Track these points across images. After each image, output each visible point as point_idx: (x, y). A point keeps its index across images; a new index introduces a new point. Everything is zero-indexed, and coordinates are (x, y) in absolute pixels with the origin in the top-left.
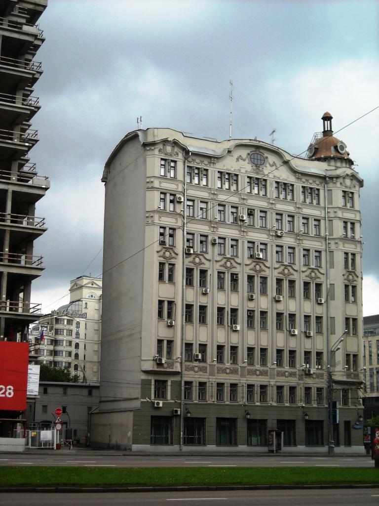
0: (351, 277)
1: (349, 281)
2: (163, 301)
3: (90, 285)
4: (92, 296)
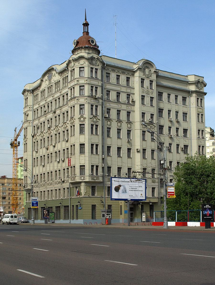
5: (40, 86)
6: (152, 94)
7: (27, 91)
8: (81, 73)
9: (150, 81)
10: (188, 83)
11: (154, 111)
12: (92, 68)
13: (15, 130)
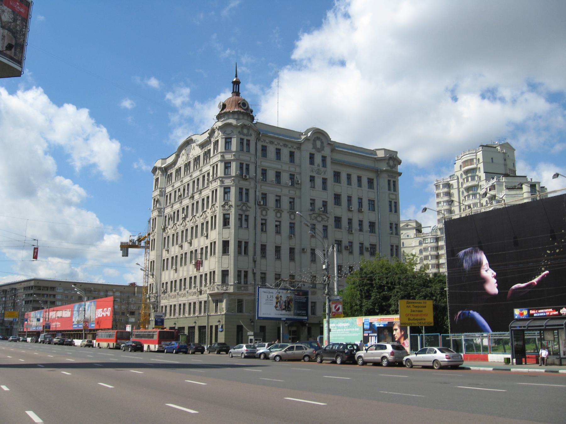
0: (244, 208)
8: (227, 145)
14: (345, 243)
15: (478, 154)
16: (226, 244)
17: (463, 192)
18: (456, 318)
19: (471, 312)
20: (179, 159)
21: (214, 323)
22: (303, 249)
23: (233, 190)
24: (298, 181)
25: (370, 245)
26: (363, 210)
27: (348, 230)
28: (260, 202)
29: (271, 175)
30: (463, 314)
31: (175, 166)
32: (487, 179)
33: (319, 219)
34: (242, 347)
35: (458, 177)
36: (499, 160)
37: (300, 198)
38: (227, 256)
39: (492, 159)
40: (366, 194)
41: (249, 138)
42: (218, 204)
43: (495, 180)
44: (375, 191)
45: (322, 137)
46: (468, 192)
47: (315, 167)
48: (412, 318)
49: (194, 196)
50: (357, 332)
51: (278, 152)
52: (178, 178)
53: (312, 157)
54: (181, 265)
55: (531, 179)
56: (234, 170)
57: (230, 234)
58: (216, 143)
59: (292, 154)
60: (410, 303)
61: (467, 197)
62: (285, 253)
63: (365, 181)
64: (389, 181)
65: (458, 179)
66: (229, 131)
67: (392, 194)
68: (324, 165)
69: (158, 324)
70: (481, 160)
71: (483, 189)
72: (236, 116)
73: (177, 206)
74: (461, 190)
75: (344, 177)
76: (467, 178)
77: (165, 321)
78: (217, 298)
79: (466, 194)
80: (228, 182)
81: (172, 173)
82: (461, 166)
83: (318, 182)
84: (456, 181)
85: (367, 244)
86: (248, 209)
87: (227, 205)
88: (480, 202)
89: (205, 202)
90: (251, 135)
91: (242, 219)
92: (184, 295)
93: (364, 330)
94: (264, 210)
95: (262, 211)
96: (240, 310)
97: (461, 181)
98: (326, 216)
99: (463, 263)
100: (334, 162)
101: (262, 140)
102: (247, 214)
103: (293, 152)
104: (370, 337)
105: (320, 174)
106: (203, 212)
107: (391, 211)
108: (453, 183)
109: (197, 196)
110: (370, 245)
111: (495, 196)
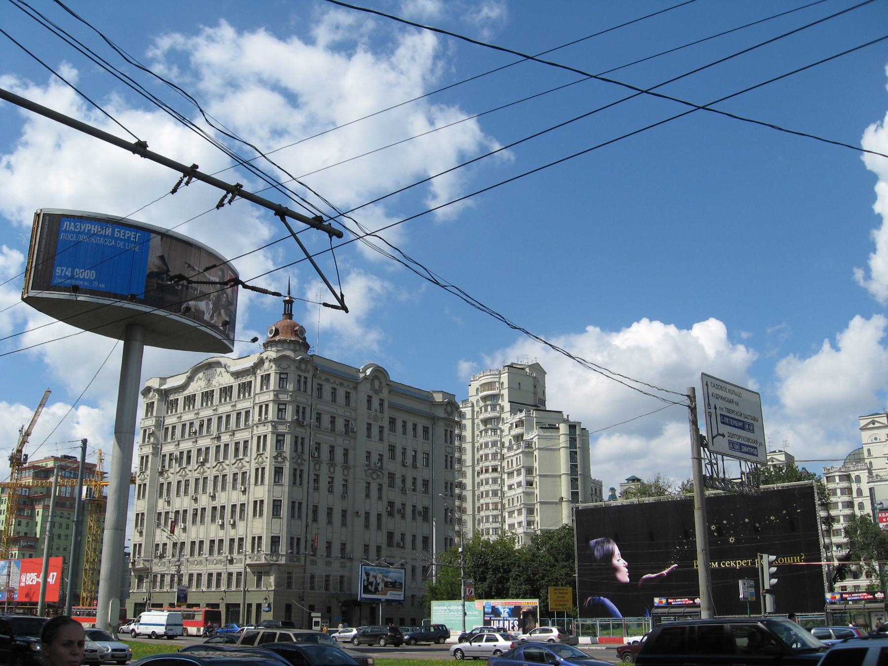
0: (299, 461)
1: (298, 464)
2: (489, 503)
3: (871, 426)
4: (876, 439)
5: (184, 387)
6: (382, 421)
7: (154, 390)
8: (281, 382)
9: (380, 399)
10: (434, 404)
11: (384, 449)
12: (300, 376)
13: (20, 431)
14: (398, 505)
15: (502, 376)
16: (276, 505)
17: (478, 425)
18: (586, 603)
19: (602, 598)
20: (192, 383)
21: (254, 600)
22: (357, 513)
23: (288, 439)
24: (353, 429)
25: (423, 507)
26: (418, 466)
27: (402, 490)
28: (314, 454)
29: (326, 421)
30: (593, 600)
31: (183, 391)
32: (513, 411)
33: (375, 476)
34: (351, 631)
35: (473, 404)
36: (528, 385)
37: (354, 449)
38: (278, 519)
39: (519, 384)
40: (422, 446)
41: (306, 375)
42: (268, 453)
43: (523, 414)
44: (430, 442)
45: (380, 376)
46: (486, 425)
47: (373, 413)
48: (558, 603)
49: (220, 436)
50: (476, 616)
51: (334, 392)
52: (189, 408)
53: (369, 400)
54: (194, 522)
55: (568, 416)
56: (289, 415)
57: (283, 492)
58: (266, 378)
59: (348, 396)
60: (557, 589)
61: (483, 432)
62: (337, 516)
63: (420, 430)
64: (446, 430)
65: (473, 406)
66: (285, 364)
67: (449, 447)
68: (382, 411)
69: (181, 600)
70: (506, 385)
71: (507, 423)
72: (292, 346)
73: (186, 446)
74: (476, 421)
75: (399, 424)
76: (486, 406)
77: (189, 594)
78: (260, 571)
79: (482, 427)
80: (282, 429)
81: (178, 399)
82: (477, 389)
83: (375, 431)
84: (470, 408)
85: (420, 508)
86: (303, 462)
87: (281, 456)
88: (501, 441)
89: (241, 448)
90: (309, 371)
91: (297, 476)
92: (200, 563)
93: (485, 613)
94: (317, 463)
95: (315, 465)
96: (289, 585)
97: (476, 409)
98: (382, 473)
99: (594, 551)
100: (392, 406)
101: (318, 377)
102: (302, 469)
103: (349, 393)
104: (492, 622)
105: (377, 422)
106: (237, 460)
107: (446, 467)
108: (466, 412)
109: (225, 438)
110: (423, 507)
111: (522, 435)
